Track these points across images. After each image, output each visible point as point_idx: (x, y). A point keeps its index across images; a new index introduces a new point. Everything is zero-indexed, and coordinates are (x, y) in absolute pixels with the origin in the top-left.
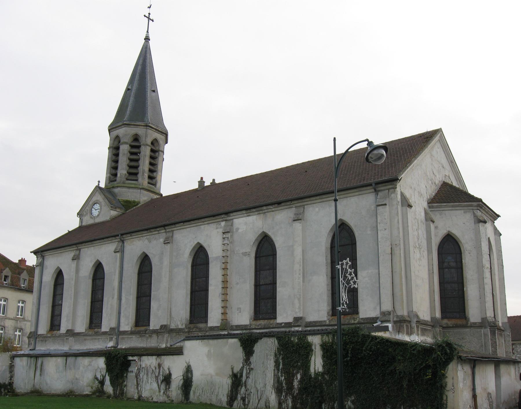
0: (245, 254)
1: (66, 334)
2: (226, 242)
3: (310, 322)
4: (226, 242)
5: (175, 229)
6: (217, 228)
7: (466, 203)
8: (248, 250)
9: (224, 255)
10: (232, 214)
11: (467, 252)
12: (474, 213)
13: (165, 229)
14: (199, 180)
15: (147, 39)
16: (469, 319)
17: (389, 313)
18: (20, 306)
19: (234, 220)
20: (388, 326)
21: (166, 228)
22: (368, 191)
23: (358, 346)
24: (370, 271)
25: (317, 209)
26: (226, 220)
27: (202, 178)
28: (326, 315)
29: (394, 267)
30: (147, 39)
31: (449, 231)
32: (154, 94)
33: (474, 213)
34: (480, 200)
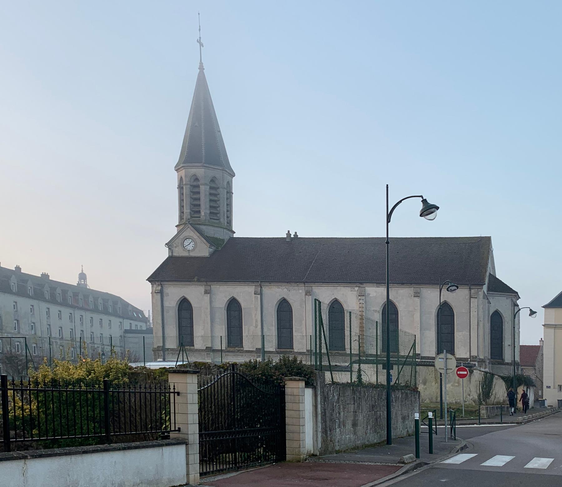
0: (375, 311)
1: (205, 349)
2: (361, 301)
3: (424, 357)
4: (361, 301)
5: (314, 285)
6: (351, 291)
7: (508, 294)
8: (378, 309)
9: (360, 310)
10: (365, 284)
11: (506, 323)
12: (512, 299)
13: (304, 284)
14: (287, 233)
15: (201, 68)
16: (505, 360)
17: (476, 357)
18: (434, 360)
19: (366, 288)
20: (475, 364)
21: (305, 283)
22: (467, 287)
23: (286, 363)
24: (463, 333)
25: (429, 292)
26: (359, 287)
27: (289, 231)
28: (435, 354)
29: (479, 333)
30: (201, 68)
31: (497, 309)
32: (219, 133)
33: (512, 299)
34: (517, 293)
